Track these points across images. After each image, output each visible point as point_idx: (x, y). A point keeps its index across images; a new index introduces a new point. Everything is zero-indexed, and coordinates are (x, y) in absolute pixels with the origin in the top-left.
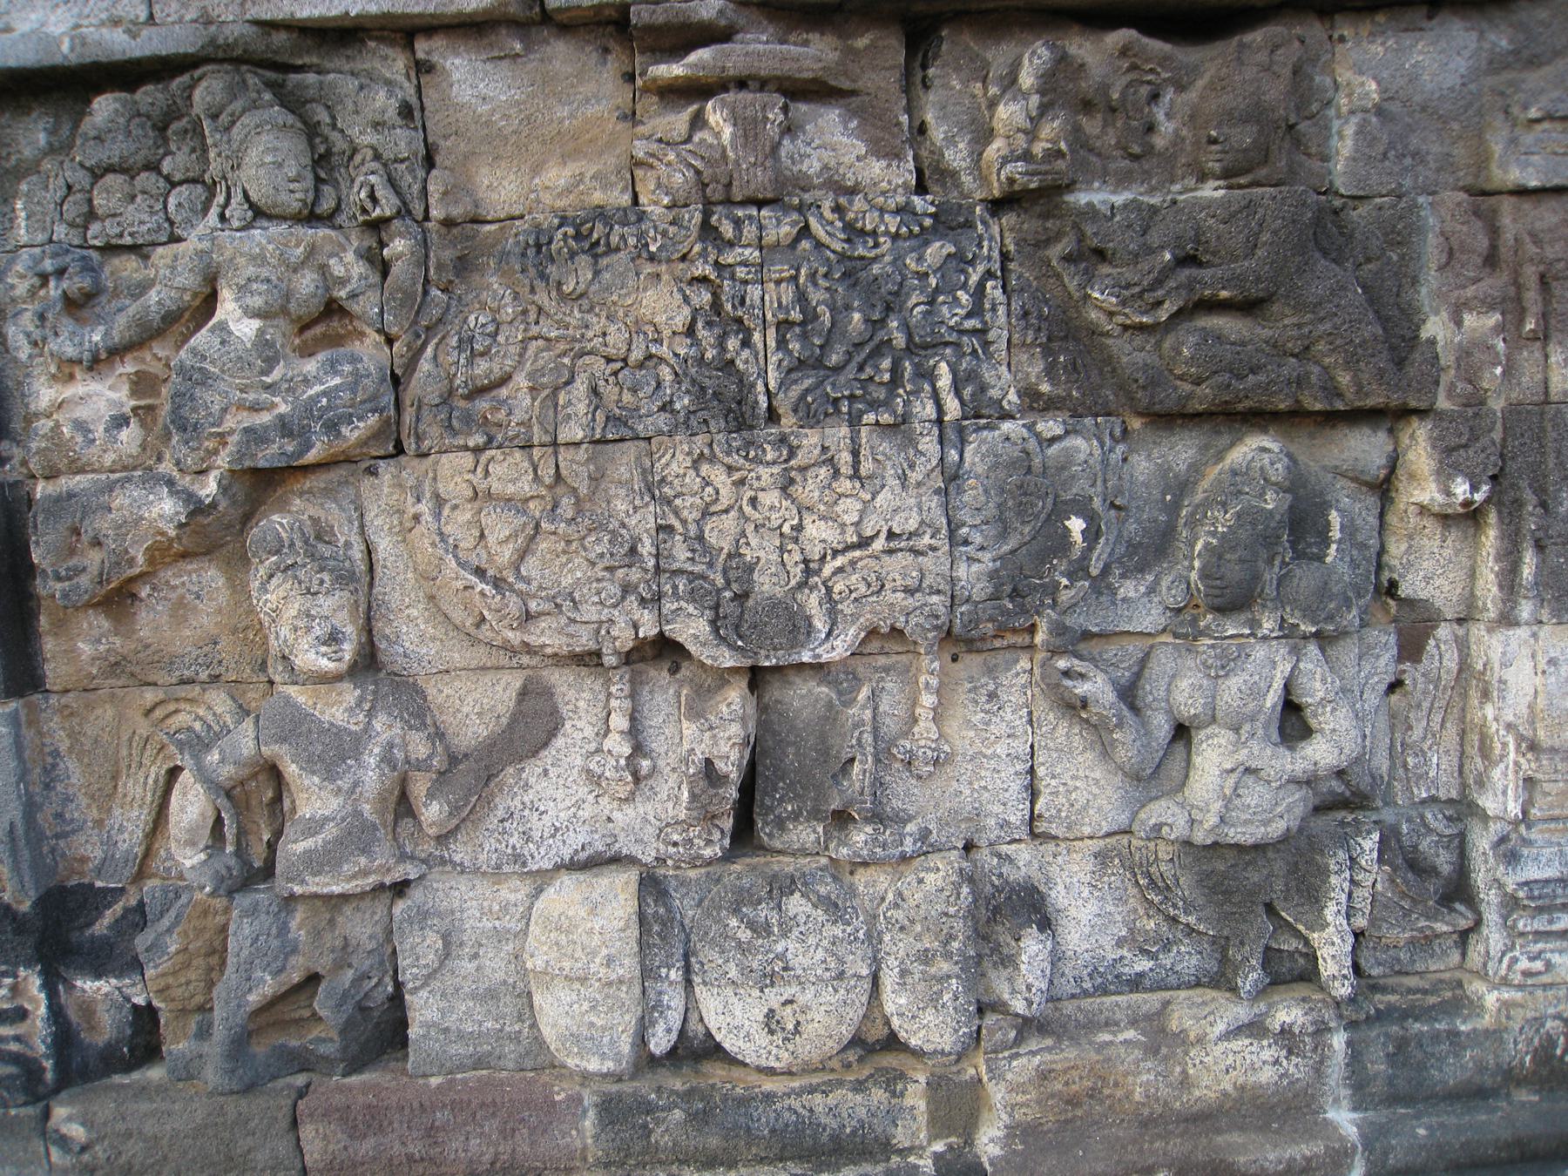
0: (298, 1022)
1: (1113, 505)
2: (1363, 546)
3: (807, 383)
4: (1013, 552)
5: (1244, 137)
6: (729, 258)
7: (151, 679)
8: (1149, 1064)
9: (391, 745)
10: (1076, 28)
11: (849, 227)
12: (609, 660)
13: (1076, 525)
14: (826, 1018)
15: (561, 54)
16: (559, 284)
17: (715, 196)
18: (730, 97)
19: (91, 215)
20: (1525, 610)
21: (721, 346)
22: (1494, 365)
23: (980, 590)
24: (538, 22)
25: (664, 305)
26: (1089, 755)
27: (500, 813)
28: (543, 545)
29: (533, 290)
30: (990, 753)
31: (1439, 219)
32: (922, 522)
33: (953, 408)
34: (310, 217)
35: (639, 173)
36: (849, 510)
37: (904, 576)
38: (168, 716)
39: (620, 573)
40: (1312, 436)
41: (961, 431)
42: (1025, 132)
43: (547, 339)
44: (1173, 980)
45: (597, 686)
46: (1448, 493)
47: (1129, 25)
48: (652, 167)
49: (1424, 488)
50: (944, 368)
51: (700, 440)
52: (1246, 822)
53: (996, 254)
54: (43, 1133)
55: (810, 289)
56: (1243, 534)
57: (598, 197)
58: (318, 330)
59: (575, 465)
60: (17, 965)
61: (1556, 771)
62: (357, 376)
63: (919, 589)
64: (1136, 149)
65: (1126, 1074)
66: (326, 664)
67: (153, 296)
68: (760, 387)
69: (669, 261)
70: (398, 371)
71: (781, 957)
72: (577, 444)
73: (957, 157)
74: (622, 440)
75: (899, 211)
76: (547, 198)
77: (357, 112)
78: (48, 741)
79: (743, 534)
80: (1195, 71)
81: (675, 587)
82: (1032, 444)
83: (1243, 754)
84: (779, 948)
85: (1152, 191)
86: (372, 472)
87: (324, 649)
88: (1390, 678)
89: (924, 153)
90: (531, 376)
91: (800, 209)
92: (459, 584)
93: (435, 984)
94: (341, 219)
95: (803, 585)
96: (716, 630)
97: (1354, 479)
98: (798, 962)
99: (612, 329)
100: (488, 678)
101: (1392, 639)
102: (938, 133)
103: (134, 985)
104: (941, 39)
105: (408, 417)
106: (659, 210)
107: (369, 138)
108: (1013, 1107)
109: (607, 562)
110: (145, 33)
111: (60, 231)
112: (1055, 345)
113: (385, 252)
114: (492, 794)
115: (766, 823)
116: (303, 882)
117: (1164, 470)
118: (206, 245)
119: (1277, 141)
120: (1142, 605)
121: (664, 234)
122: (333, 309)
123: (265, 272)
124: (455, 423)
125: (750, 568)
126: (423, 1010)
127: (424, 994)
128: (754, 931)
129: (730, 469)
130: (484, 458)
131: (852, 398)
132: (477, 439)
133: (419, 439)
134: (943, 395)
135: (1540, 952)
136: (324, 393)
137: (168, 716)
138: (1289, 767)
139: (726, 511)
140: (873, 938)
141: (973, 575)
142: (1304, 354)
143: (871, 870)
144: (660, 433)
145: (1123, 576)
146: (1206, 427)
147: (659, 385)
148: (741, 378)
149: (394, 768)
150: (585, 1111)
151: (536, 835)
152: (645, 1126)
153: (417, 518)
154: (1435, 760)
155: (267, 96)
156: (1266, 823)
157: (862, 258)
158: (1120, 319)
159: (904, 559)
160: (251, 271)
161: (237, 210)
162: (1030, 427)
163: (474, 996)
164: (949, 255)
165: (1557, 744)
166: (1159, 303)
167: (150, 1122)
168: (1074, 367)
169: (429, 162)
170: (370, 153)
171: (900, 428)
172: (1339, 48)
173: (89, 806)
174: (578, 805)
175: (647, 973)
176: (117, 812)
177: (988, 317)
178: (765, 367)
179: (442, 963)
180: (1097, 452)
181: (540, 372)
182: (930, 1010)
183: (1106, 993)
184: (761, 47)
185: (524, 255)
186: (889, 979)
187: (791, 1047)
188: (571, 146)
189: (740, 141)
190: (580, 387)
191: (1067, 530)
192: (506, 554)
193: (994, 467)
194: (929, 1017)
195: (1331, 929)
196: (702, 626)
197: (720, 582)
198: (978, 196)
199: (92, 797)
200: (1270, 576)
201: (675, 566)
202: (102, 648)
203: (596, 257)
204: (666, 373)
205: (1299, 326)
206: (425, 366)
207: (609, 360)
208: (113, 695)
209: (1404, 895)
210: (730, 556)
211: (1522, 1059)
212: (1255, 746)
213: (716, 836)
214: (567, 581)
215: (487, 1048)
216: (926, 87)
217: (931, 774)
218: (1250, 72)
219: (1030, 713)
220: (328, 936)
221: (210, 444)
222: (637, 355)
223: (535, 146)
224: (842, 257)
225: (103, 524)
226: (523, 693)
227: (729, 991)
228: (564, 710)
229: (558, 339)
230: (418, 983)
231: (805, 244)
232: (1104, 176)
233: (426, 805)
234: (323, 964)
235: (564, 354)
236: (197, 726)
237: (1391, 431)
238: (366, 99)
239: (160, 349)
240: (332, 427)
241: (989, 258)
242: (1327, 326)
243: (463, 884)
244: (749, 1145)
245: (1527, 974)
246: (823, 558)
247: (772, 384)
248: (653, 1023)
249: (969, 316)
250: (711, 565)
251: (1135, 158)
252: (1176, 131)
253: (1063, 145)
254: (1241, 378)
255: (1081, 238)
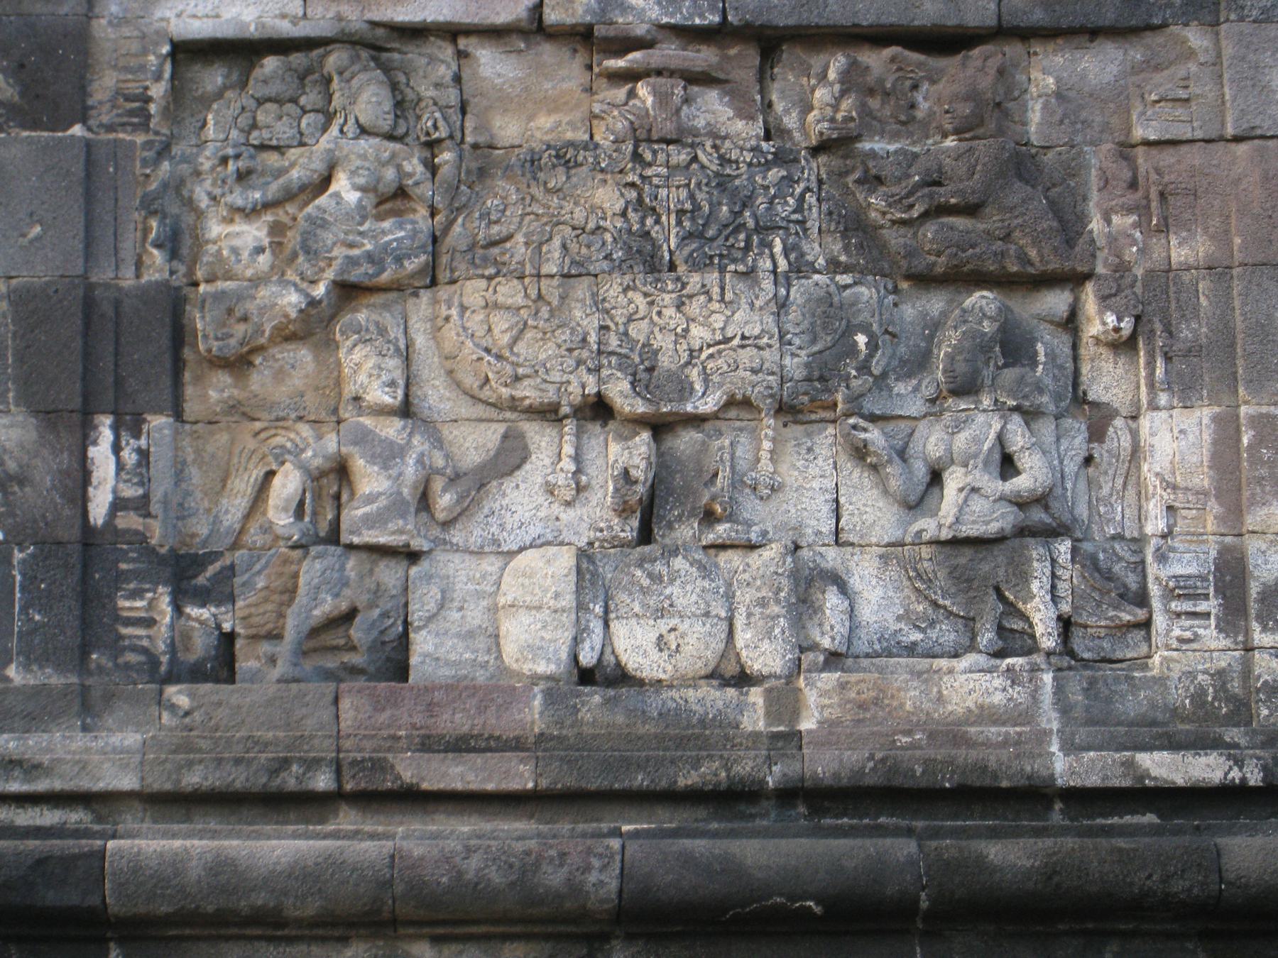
0: (335, 649)
1: (887, 332)
2: (1061, 367)
3: (694, 246)
4: (820, 352)
5: (966, 109)
6: (649, 172)
7: (256, 416)
8: (915, 684)
9: (422, 454)
10: (867, 46)
11: (721, 157)
12: (565, 410)
13: (861, 339)
14: (698, 644)
15: (548, 52)
16: (545, 183)
17: (642, 137)
18: (652, 80)
19: (254, 126)
20: (1163, 399)
21: (642, 222)
22: (1132, 245)
23: (799, 374)
24: (535, 29)
25: (609, 198)
26: (875, 491)
27: (486, 511)
28: (529, 335)
29: (529, 186)
30: (809, 484)
31: (1098, 159)
32: (763, 330)
33: (783, 265)
34: (390, 137)
35: (595, 122)
36: (718, 321)
37: (751, 362)
38: (268, 438)
39: (576, 353)
40: (1024, 297)
41: (788, 279)
42: (831, 106)
43: (537, 215)
44: (937, 649)
45: (554, 433)
46: (1104, 324)
47: (897, 44)
48: (603, 119)
49: (1099, 321)
50: (778, 240)
51: (627, 278)
52: (974, 522)
53: (813, 178)
54: (159, 703)
55: (697, 192)
56: (967, 344)
57: (569, 135)
58: (388, 206)
59: (551, 289)
60: (158, 584)
61: (1188, 502)
62: (415, 232)
63: (760, 370)
64: (903, 118)
65: (899, 690)
66: (388, 400)
67: (295, 174)
68: (665, 247)
69: (613, 173)
70: (438, 233)
71: (669, 597)
72: (552, 276)
73: (791, 121)
74: (580, 275)
75: (752, 150)
76: (538, 135)
77: (425, 77)
78: (180, 453)
79: (652, 332)
80: (942, 72)
81: (610, 362)
82: (833, 288)
83: (969, 479)
84: (668, 591)
85: (914, 143)
86: (416, 295)
87: (387, 389)
88: (1084, 454)
89: (771, 119)
90: (526, 235)
91: (692, 146)
92: (475, 357)
93: (432, 626)
94: (409, 140)
95: (688, 363)
96: (634, 387)
97: (1052, 322)
98: (680, 602)
99: (577, 210)
100: (483, 426)
101: (1083, 427)
102: (779, 107)
103: (226, 613)
104: (782, 51)
105: (444, 259)
106: (607, 143)
107: (431, 93)
108: (823, 707)
109: (568, 345)
110: (302, 23)
111: (234, 134)
112: (850, 234)
113: (436, 160)
114: (482, 499)
115: (660, 528)
116: (360, 534)
117: (924, 314)
118: (332, 146)
119: (990, 113)
120: (908, 397)
121: (610, 157)
122: (401, 193)
123: (367, 164)
124: (477, 261)
125: (656, 352)
126: (423, 644)
127: (424, 633)
128: (652, 579)
129: (646, 295)
130: (494, 283)
131: (721, 256)
132: (491, 271)
133: (452, 271)
134: (777, 257)
135: (1191, 627)
136: (395, 240)
137: (268, 438)
138: (1000, 488)
139: (642, 319)
140: (729, 597)
141: (794, 365)
142: (1007, 238)
143: (730, 553)
144: (604, 272)
145: (897, 380)
146: (951, 288)
147: (604, 244)
148: (653, 242)
149: (424, 468)
150: (535, 696)
151: (509, 527)
152: (575, 706)
153: (447, 319)
154: (1119, 509)
155: (372, 64)
156: (987, 523)
157: (729, 176)
158: (889, 216)
159: (751, 351)
160: (358, 163)
161: (351, 128)
162: (832, 280)
163: (458, 635)
164: (783, 177)
165: (1190, 485)
166: (911, 206)
167: (236, 696)
168: (860, 246)
169: (463, 111)
170: (431, 102)
171: (749, 274)
172: (1033, 59)
173: (202, 499)
174: (537, 508)
175: (581, 607)
176: (225, 501)
177: (806, 213)
178: (669, 237)
179: (439, 610)
180: (875, 296)
181: (532, 233)
182: (766, 641)
183: (890, 655)
184: (671, 52)
185: (523, 166)
186: (740, 622)
187: (673, 661)
188: (553, 105)
189: (657, 106)
190: (557, 242)
191: (856, 343)
192: (506, 339)
193: (809, 300)
194: (765, 645)
195: (1037, 599)
196: (625, 385)
197: (637, 360)
198: (804, 145)
199: (206, 494)
200: (987, 373)
201: (610, 349)
202: (225, 395)
203: (569, 168)
204: (608, 237)
205: (1003, 221)
206: (457, 228)
207: (574, 228)
208: (229, 427)
209: (1094, 588)
210: (644, 346)
211: (1183, 702)
212: (977, 473)
213: (628, 528)
214: (542, 356)
215: (464, 672)
216: (773, 80)
217: (769, 497)
218: (970, 71)
219: (835, 463)
220: (367, 580)
221: (322, 264)
222: (591, 225)
223: (529, 105)
224: (717, 174)
225: (251, 307)
226: (505, 437)
227: (634, 621)
228: (532, 447)
229: (542, 215)
230: (421, 623)
231: (695, 166)
232: (882, 134)
233: (441, 496)
234: (362, 600)
235: (546, 224)
236: (289, 445)
237: (1072, 290)
238: (431, 70)
239: (291, 208)
240: (399, 260)
241: (808, 180)
242: (1020, 221)
243: (457, 558)
244: (644, 723)
245: (1181, 640)
246: (701, 349)
247: (673, 246)
248: (583, 641)
249: (794, 212)
250: (632, 350)
251: (903, 123)
252: (930, 108)
253: (854, 114)
254: (964, 251)
255: (866, 171)
